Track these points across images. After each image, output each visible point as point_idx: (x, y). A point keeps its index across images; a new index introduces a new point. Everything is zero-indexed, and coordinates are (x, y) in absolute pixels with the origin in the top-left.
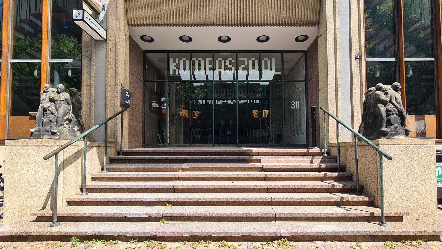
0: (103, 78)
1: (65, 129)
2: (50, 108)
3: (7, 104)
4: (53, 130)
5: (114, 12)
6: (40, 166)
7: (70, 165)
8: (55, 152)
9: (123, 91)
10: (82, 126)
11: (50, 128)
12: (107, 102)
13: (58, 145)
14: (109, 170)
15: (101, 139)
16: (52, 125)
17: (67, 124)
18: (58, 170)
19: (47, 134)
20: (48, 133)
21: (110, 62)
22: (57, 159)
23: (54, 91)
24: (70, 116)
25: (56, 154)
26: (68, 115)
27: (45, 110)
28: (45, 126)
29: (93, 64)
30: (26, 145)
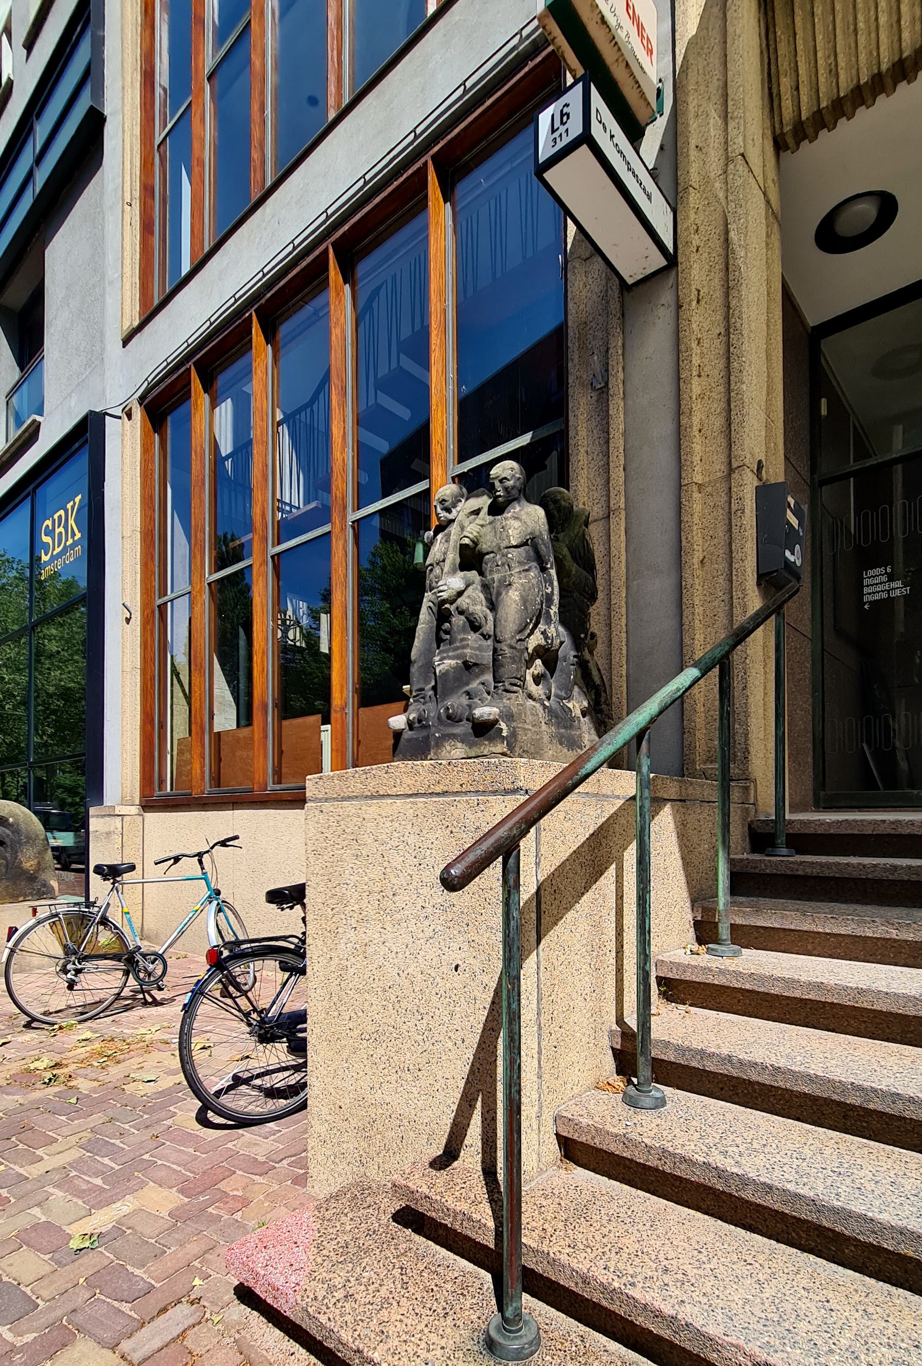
0: (664, 456)
1: (529, 703)
2: (463, 602)
3: (347, 668)
4: (485, 711)
5: (715, 84)
6: (430, 910)
7: (570, 915)
8: (502, 832)
9: (768, 497)
10: (598, 695)
11: (464, 700)
12: (687, 574)
13: (507, 792)
14: (745, 937)
15: (680, 761)
16: (474, 685)
17: (537, 680)
18: (517, 943)
19: (453, 736)
20: (457, 730)
21: (696, 360)
22: (511, 882)
23: (477, 512)
24: (552, 631)
25: (507, 850)
26: (542, 627)
27: (442, 615)
28: (445, 696)
29: (617, 407)
30: (372, 797)
